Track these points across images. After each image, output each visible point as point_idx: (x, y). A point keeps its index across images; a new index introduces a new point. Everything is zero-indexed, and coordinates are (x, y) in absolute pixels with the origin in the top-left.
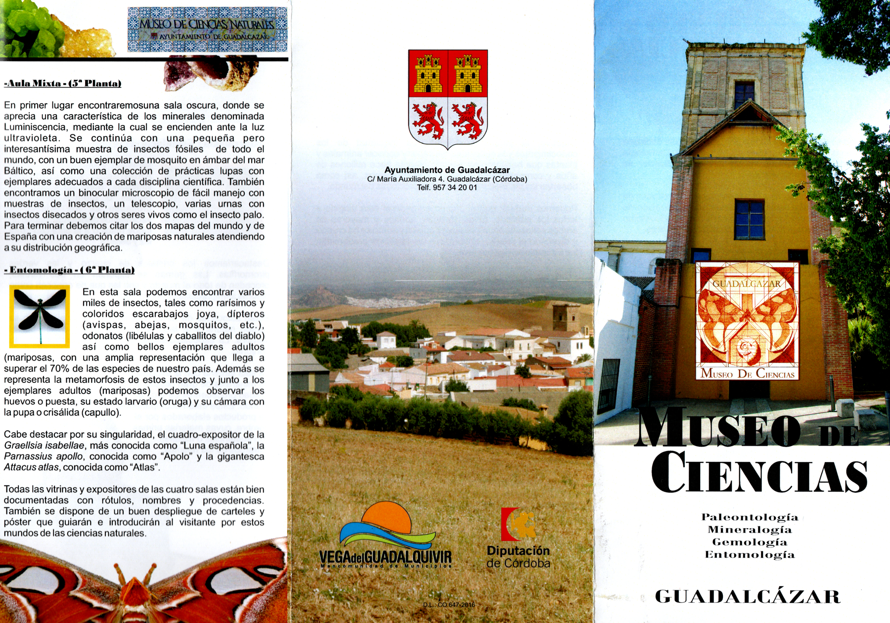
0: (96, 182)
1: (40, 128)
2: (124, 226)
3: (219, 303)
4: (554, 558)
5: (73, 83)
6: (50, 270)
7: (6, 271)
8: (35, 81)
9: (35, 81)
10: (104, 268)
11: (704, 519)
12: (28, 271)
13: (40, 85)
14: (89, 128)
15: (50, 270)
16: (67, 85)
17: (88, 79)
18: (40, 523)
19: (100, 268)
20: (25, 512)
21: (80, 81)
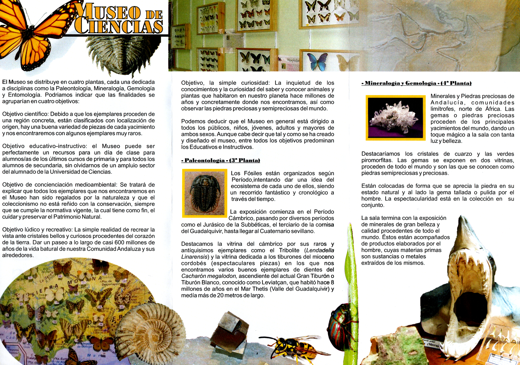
0: (420, 244)
1: (246, 276)
2: (248, 289)
3: (315, 244)
4: (113, 44)
5: (232, 160)
6: (211, 161)
7: (182, 161)
8: (366, 82)
9: (366, 82)
10: (242, 159)
11: (259, 159)
12: (208, 161)
13: (369, 84)
14: (85, 185)
15: (211, 161)
16: (229, 162)
17: (241, 158)
18: (50, 198)
19: (451, 82)
20: (100, 185)
21: (236, 159)
